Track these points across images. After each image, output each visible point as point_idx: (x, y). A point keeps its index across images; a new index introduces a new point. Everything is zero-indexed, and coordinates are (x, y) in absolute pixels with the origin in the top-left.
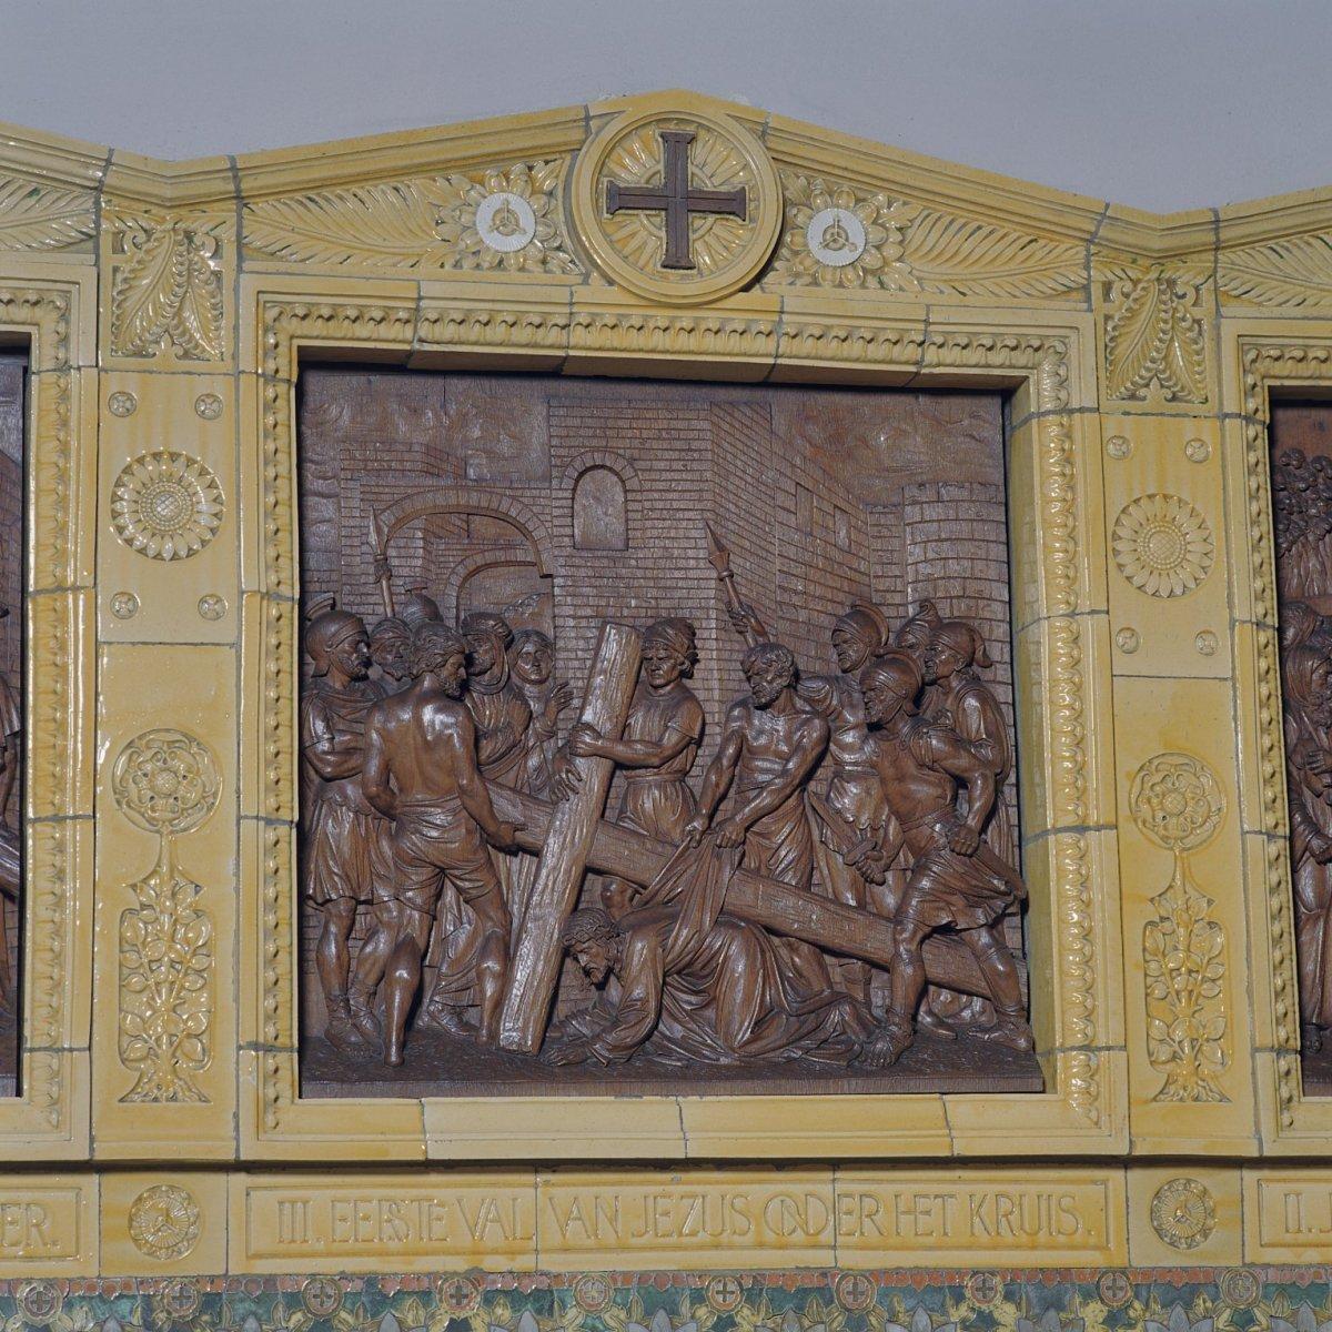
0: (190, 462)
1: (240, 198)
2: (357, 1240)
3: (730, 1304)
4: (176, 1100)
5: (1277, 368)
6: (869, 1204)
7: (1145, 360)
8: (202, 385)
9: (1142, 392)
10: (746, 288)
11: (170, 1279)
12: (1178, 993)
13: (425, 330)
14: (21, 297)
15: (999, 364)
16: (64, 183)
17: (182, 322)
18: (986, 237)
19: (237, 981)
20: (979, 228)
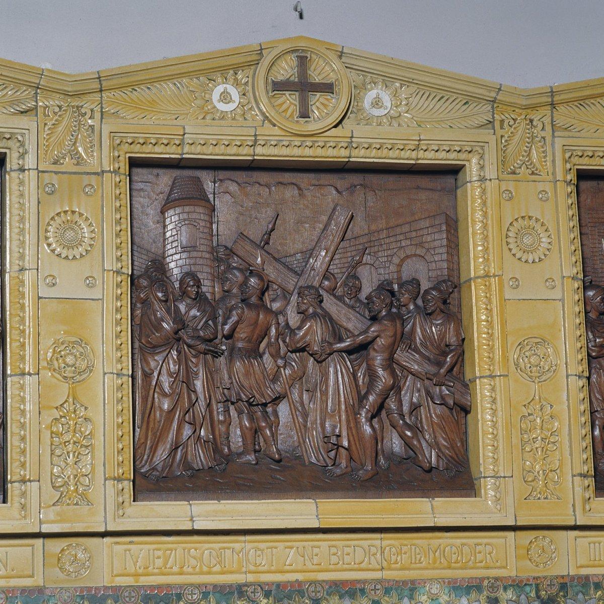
0: (537, 220)
1: (553, 105)
2: (355, 564)
3: (195, 599)
4: (547, 499)
5: (581, 161)
6: (334, 550)
7: (520, 156)
8: (541, 186)
9: (518, 171)
10: (335, 126)
11: (545, 578)
12: (68, 453)
13: (259, 150)
14: (293, 144)
15: (451, 159)
16: (479, 99)
17: (76, 148)
18: (439, 100)
19: (571, 447)
20: (442, 97)
